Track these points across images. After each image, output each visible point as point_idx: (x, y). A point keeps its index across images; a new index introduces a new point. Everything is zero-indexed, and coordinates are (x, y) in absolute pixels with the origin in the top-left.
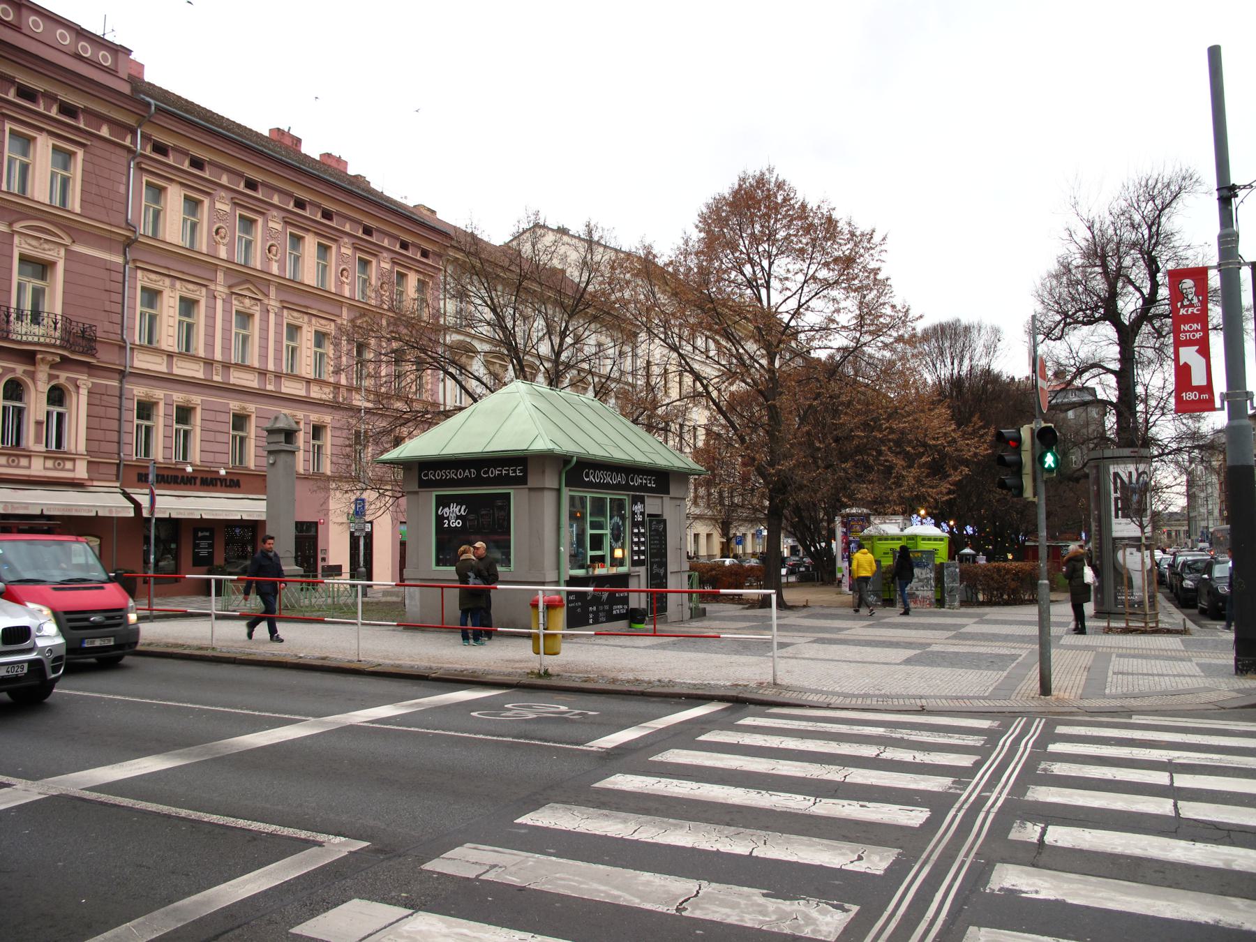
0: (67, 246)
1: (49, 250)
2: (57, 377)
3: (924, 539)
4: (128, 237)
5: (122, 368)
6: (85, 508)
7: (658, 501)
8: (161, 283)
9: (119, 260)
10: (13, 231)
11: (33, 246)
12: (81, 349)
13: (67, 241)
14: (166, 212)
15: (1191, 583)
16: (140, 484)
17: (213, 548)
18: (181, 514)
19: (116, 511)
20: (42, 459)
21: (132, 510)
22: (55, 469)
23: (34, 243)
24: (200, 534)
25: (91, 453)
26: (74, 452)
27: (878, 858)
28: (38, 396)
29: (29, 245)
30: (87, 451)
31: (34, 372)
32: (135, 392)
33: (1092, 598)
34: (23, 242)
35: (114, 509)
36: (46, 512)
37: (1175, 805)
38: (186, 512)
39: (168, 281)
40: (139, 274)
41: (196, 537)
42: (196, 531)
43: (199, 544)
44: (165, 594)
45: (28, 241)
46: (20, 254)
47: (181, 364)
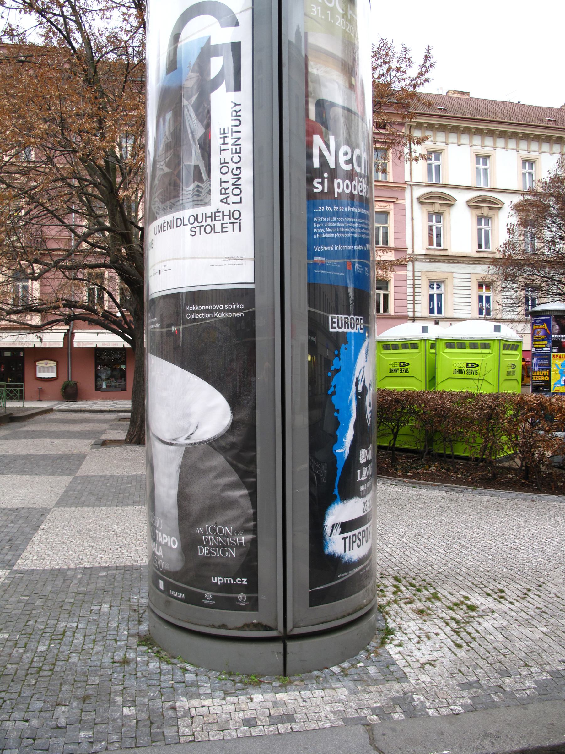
3: (450, 345)
15: (37, 294)
18: (106, 345)
19: (19, 344)
21: (62, 343)
27: (231, 686)
33: (327, 314)
35: (48, 343)
36: (99, 346)
37: (410, 133)
38: (111, 343)
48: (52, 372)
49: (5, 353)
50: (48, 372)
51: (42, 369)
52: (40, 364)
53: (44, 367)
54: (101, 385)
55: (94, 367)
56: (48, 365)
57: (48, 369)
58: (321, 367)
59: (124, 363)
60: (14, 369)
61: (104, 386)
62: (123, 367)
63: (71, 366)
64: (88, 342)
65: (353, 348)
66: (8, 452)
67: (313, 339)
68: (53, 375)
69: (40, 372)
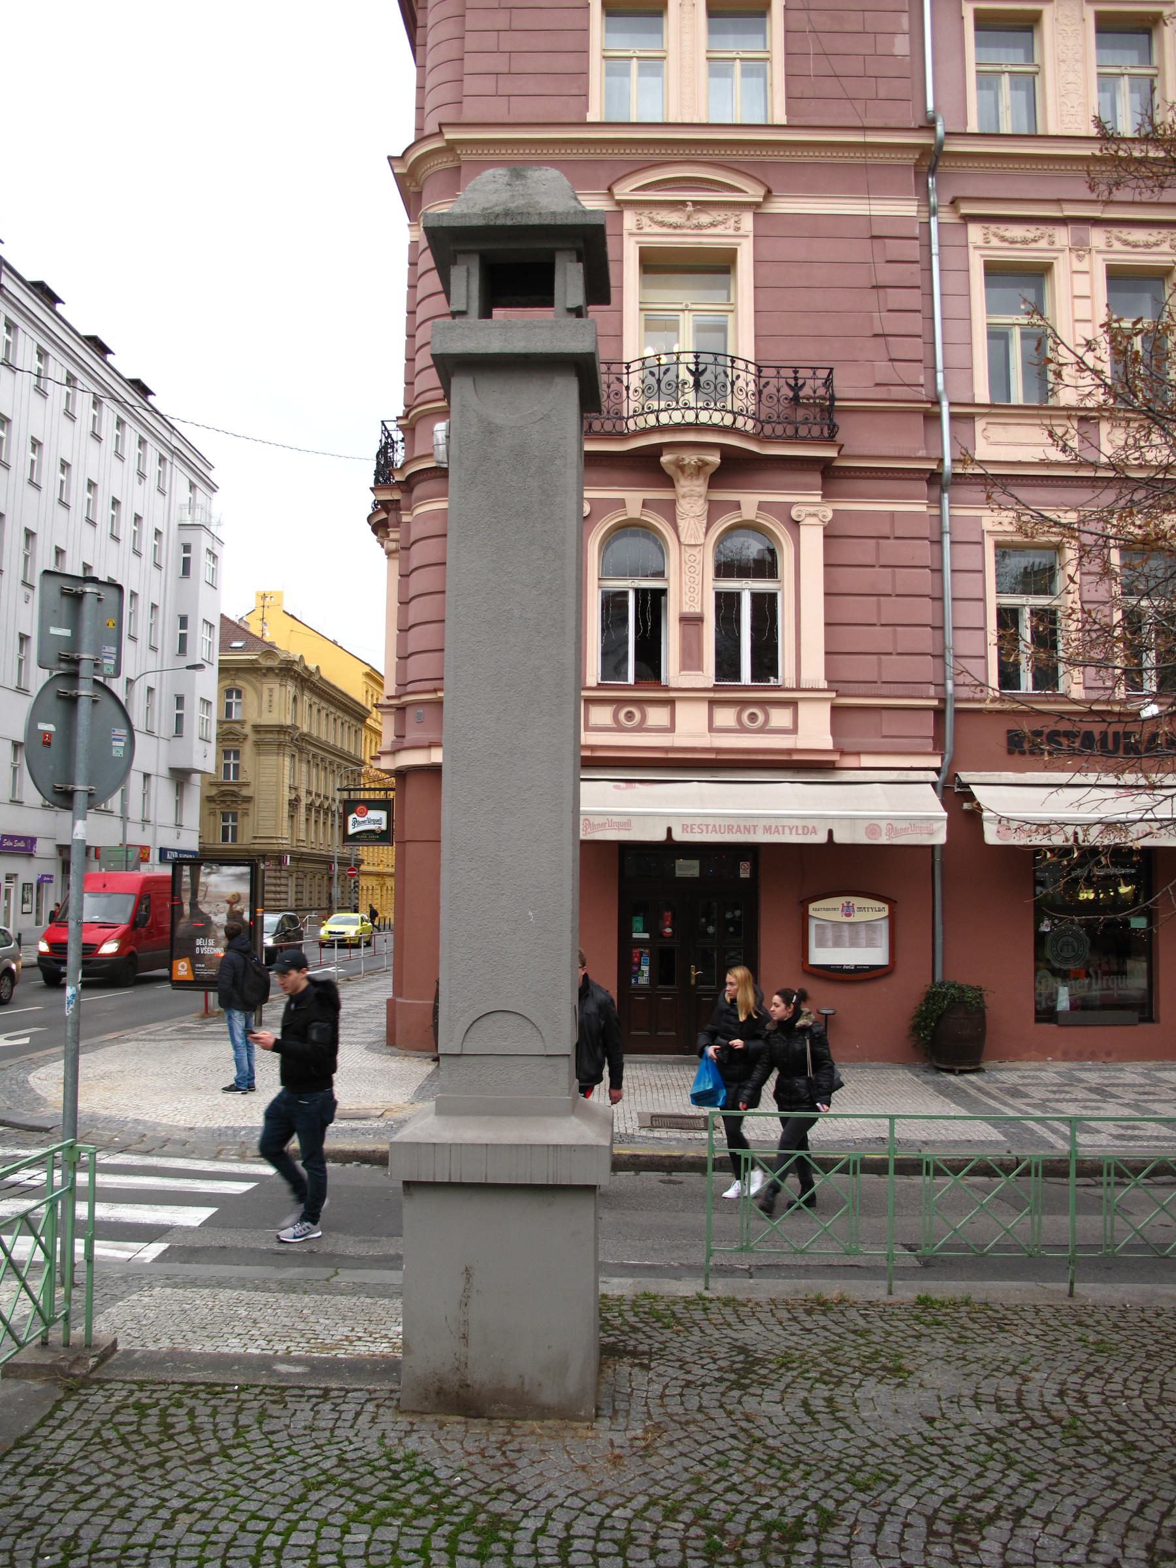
0: (758, 205)
1: (713, 225)
2: (737, 506)
4: (924, 149)
5: (933, 466)
6: (795, 822)
7: (575, 465)
8: (1043, 244)
9: (908, 208)
10: (619, 203)
11: (670, 226)
12: (790, 431)
13: (754, 193)
16: (1016, 757)
20: (704, 707)
21: (943, 825)
22: (742, 729)
23: (674, 217)
25: (836, 686)
26: (790, 682)
28: (685, 556)
29: (662, 224)
30: (829, 682)
31: (673, 503)
32: (987, 525)
34: (645, 221)
39: (1062, 236)
40: (975, 232)
44: (1108, 1054)
45: (659, 218)
46: (986, 263)
47: (997, 433)
48: (871, 944)
50: (854, 944)
51: (829, 934)
52: (825, 911)
53: (837, 924)
55: (1032, 924)
56: (857, 917)
57: (853, 934)
63: (944, 923)
64: (627, 819)
67: (966, 806)
68: (875, 955)
69: (821, 944)
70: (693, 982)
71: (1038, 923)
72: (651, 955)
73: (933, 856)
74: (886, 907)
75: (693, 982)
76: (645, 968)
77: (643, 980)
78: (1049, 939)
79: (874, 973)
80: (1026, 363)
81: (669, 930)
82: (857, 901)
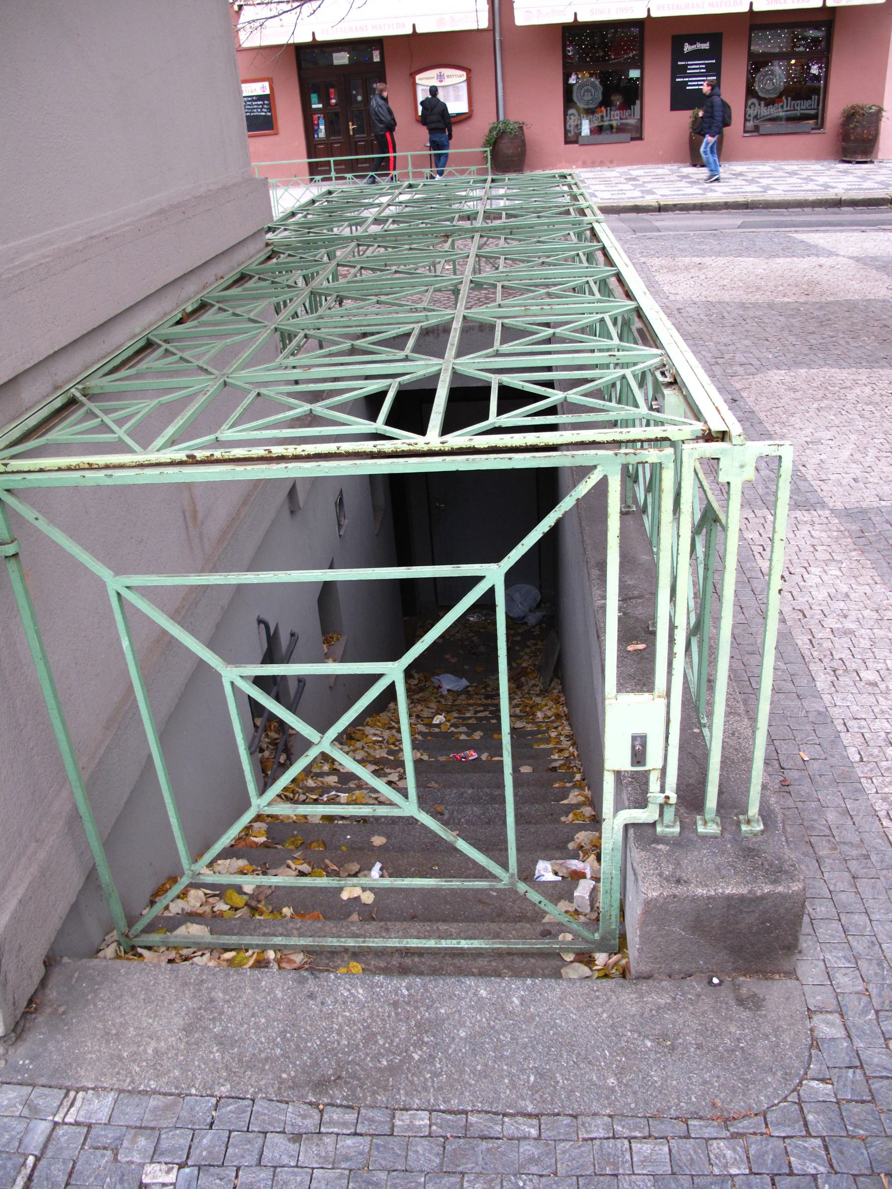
14: (853, 213)
17: (718, 76)
24: (687, 48)
41: (677, 54)
42: (677, 42)
43: (685, 67)
44: (611, 162)
49: (335, 55)
54: (578, 126)
56: (447, 82)
58: (91, 467)
59: (641, 66)
60: (359, 98)
61: (586, 130)
62: (634, 74)
65: (279, 162)
66: (651, 192)
70: (351, 133)
71: (566, 77)
72: (324, 118)
73: (494, 37)
74: (464, 73)
75: (351, 133)
76: (322, 127)
77: (322, 134)
78: (575, 88)
79: (459, 118)
80: (722, 571)
81: (333, 101)
82: (446, 72)
